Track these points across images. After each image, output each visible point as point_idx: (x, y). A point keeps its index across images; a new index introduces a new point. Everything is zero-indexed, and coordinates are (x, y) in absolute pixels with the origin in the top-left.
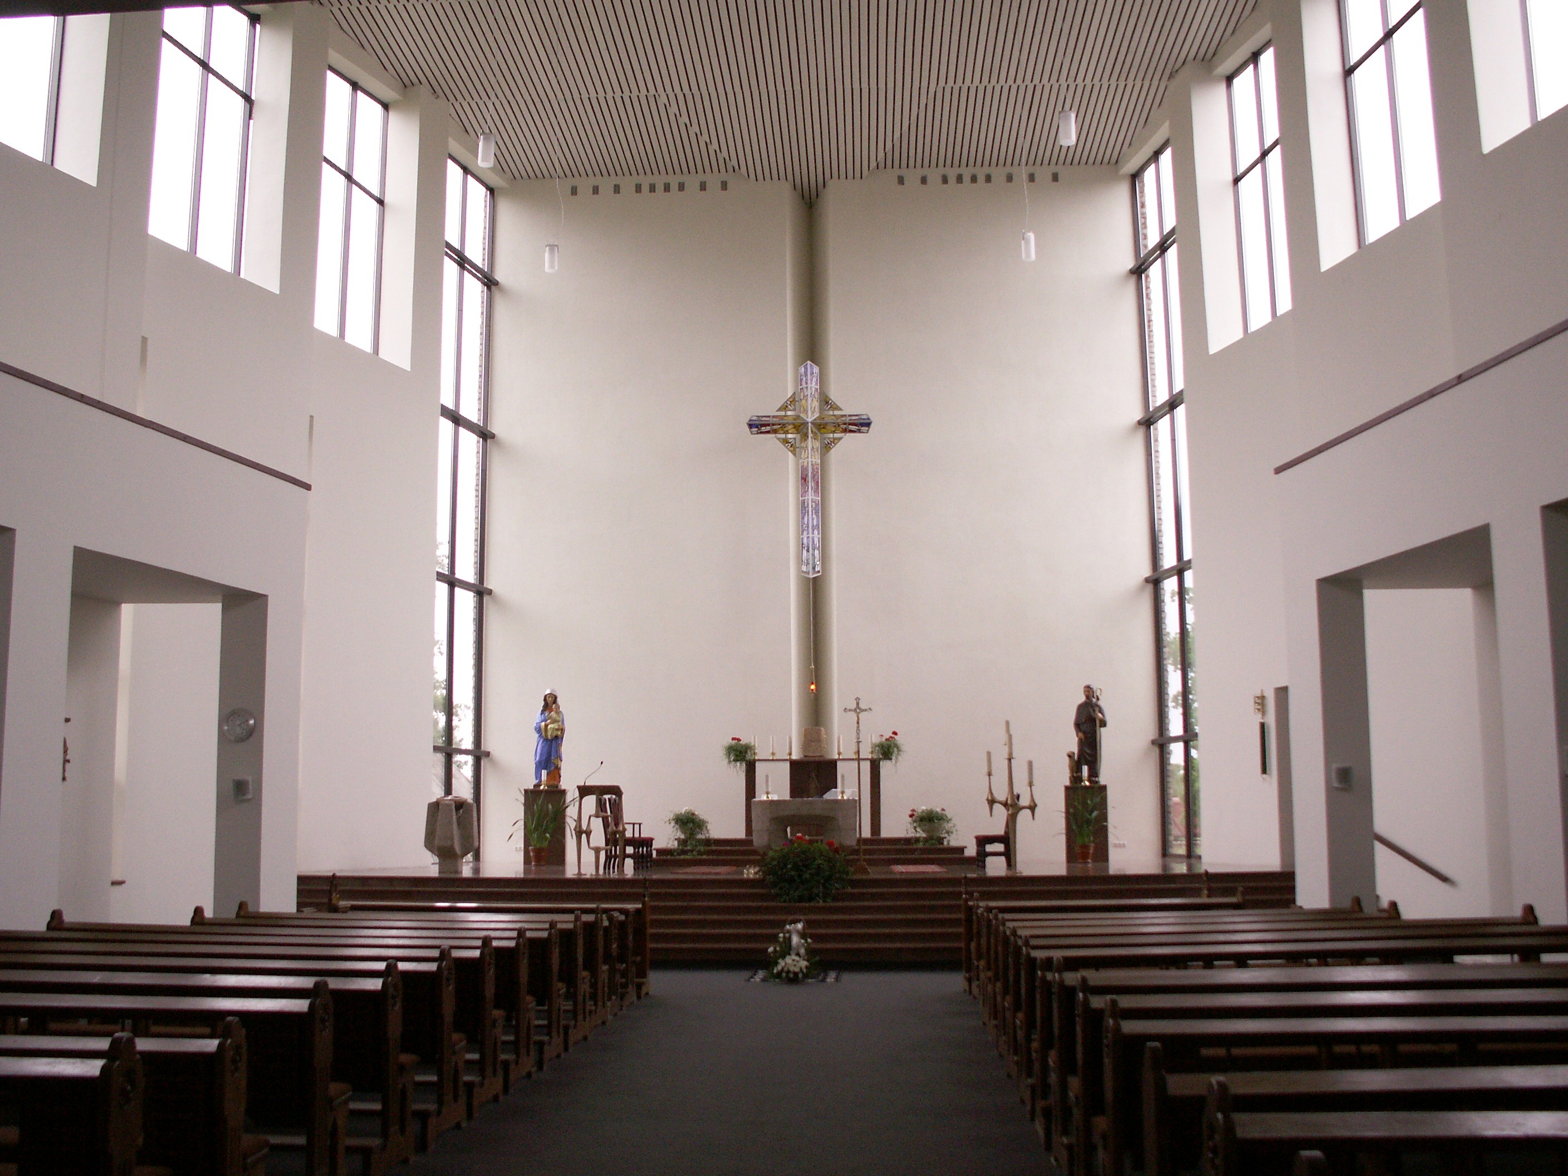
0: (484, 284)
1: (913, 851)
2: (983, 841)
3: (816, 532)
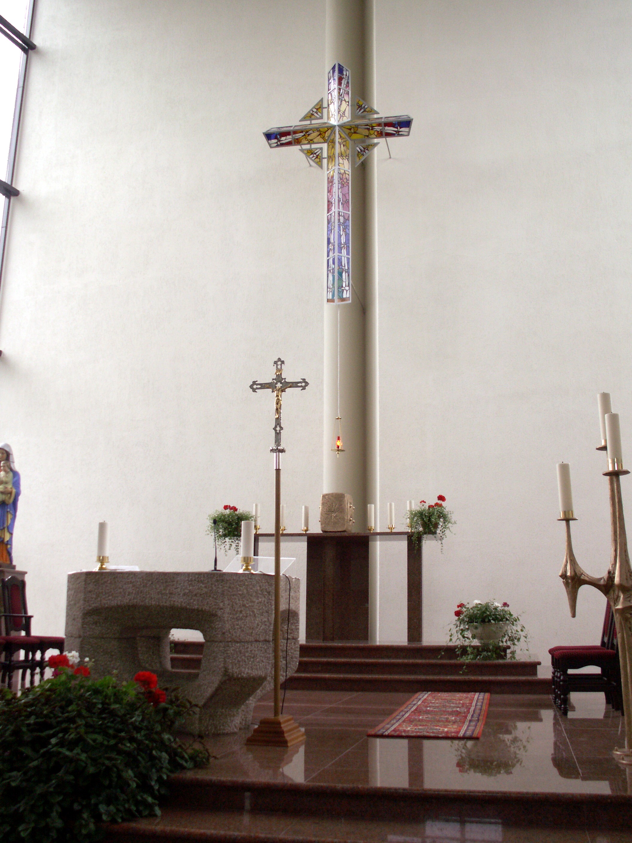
0: (23, 49)
1: (457, 668)
2: (564, 658)
3: (344, 251)
